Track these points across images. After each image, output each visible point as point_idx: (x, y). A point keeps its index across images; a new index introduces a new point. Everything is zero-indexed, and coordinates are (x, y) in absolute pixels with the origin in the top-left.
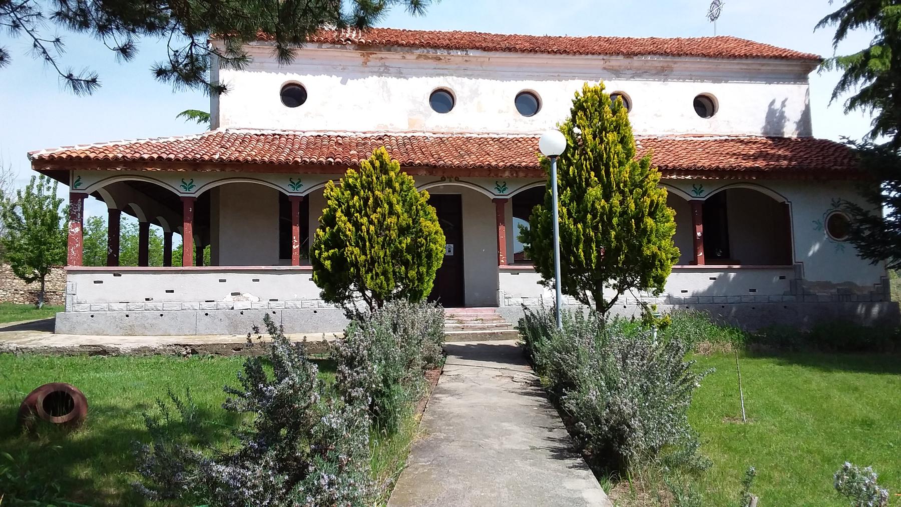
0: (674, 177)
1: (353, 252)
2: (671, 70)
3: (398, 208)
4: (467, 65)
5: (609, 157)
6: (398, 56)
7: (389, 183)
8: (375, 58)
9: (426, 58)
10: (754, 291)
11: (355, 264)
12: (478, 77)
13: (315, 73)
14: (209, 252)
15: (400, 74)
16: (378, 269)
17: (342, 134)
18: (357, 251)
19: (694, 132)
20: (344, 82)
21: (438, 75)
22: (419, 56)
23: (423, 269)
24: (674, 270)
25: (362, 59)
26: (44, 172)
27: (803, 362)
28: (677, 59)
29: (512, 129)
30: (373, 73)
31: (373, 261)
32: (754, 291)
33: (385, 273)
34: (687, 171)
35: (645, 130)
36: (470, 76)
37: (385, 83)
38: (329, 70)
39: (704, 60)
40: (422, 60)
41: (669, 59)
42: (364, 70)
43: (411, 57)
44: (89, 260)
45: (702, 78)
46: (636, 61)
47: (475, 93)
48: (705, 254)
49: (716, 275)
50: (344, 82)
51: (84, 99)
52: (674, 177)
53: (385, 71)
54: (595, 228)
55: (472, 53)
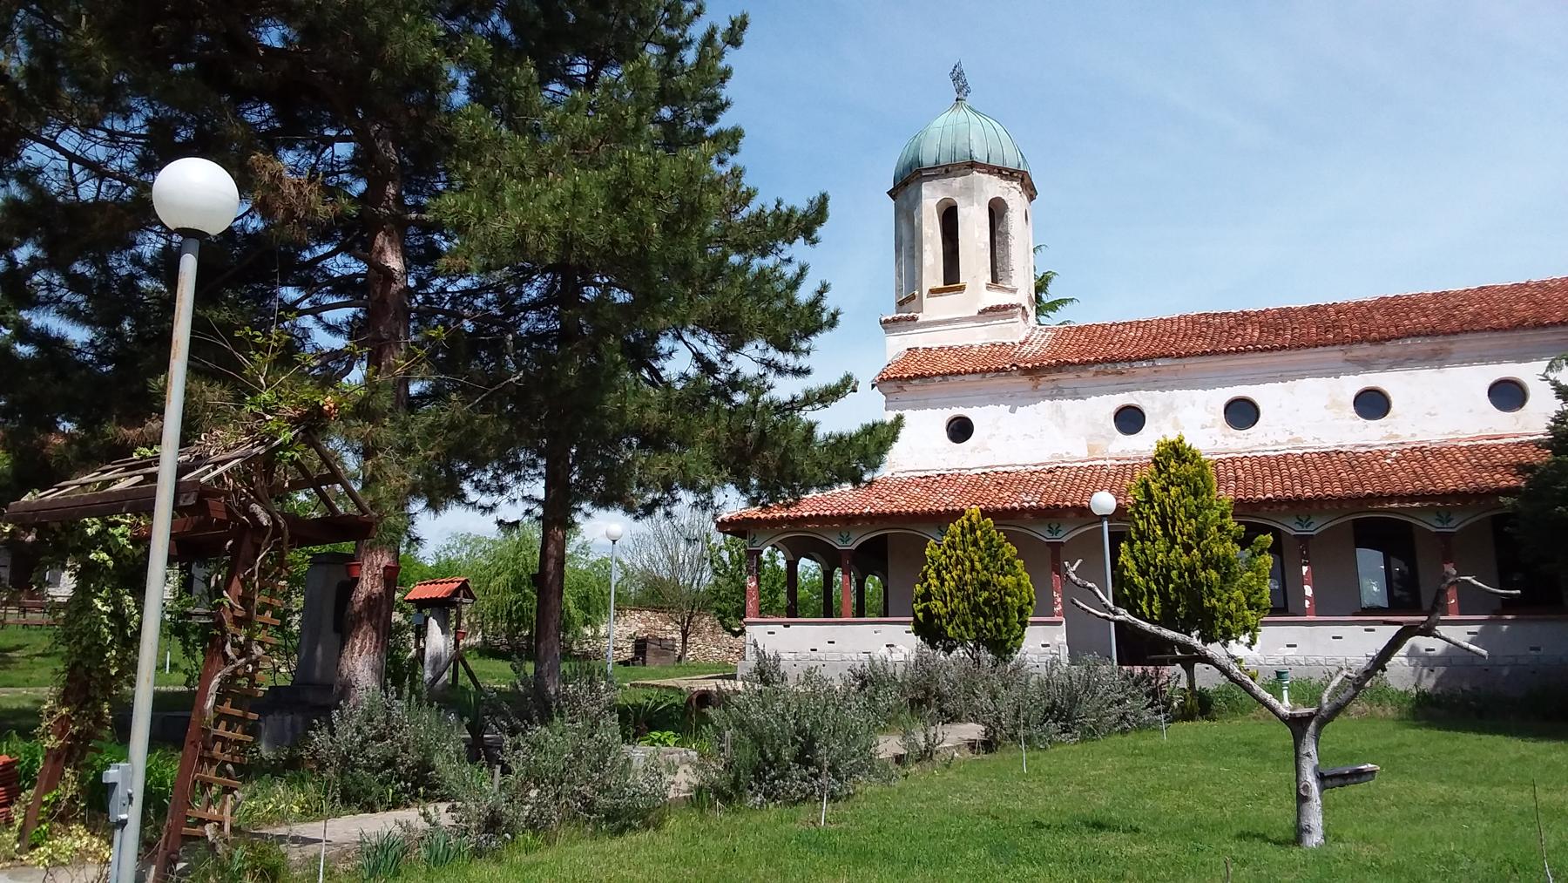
0: (1395, 505)
1: (937, 606)
2: (1450, 352)
3: (978, 566)
4: (1157, 376)
5: (1173, 512)
6: (1071, 376)
7: (975, 543)
8: (1045, 382)
9: (1105, 373)
10: (1538, 649)
11: (939, 616)
12: (1172, 388)
13: (982, 404)
14: (134, 666)
15: (1076, 395)
16: (957, 620)
17: (1009, 469)
18: (940, 604)
19: (1491, 433)
20: (1012, 411)
21: (1123, 391)
22: (1097, 373)
23: (1000, 621)
24: (1033, 623)
25: (1032, 383)
26: (725, 533)
27: (1494, 731)
28: (1452, 338)
29: (1220, 447)
30: (1044, 397)
31: (953, 614)
32: (1538, 649)
33: (965, 624)
34: (1412, 497)
35: (1413, 435)
36: (1162, 389)
37: (1059, 408)
38: (996, 399)
39: (1496, 335)
40: (1101, 377)
41: (1439, 339)
42: (1033, 397)
43: (1087, 375)
44: (767, 610)
45: (1499, 359)
46: (1391, 348)
47: (1170, 407)
48: (1459, 600)
49: (1476, 628)
50: (1012, 411)
51: (969, 77)
52: (1395, 505)
53: (1058, 393)
54: (1157, 582)
55: (1159, 363)
